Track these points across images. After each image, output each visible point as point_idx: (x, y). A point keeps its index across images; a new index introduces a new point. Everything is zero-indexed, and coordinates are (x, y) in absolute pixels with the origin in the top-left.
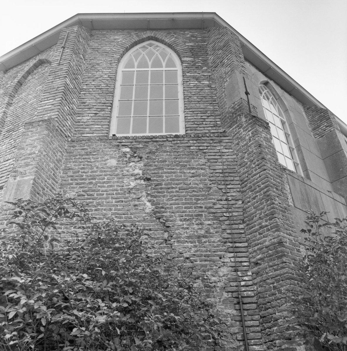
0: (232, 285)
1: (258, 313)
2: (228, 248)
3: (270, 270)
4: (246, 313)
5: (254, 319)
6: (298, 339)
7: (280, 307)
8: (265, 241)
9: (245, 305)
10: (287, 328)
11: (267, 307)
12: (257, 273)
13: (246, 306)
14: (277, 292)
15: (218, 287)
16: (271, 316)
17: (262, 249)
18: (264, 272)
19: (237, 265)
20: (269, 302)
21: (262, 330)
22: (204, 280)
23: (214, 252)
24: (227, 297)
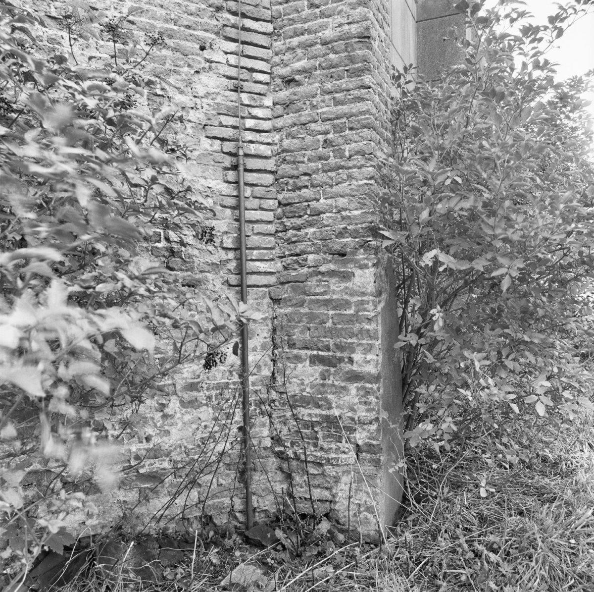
0: (224, 123)
1: (274, 195)
2: (225, 26)
3: (323, 101)
4: (248, 191)
5: (265, 206)
6: (362, 256)
7: (331, 186)
8: (323, 27)
9: (249, 174)
10: (341, 233)
11: (300, 184)
12: (287, 105)
13: (251, 178)
14: (331, 154)
15: (190, 121)
16: (306, 204)
17: (311, 45)
18: (308, 103)
19: (242, 77)
20: (305, 174)
21: (277, 232)
22: (154, 98)
23: (188, 27)
24: (210, 149)
